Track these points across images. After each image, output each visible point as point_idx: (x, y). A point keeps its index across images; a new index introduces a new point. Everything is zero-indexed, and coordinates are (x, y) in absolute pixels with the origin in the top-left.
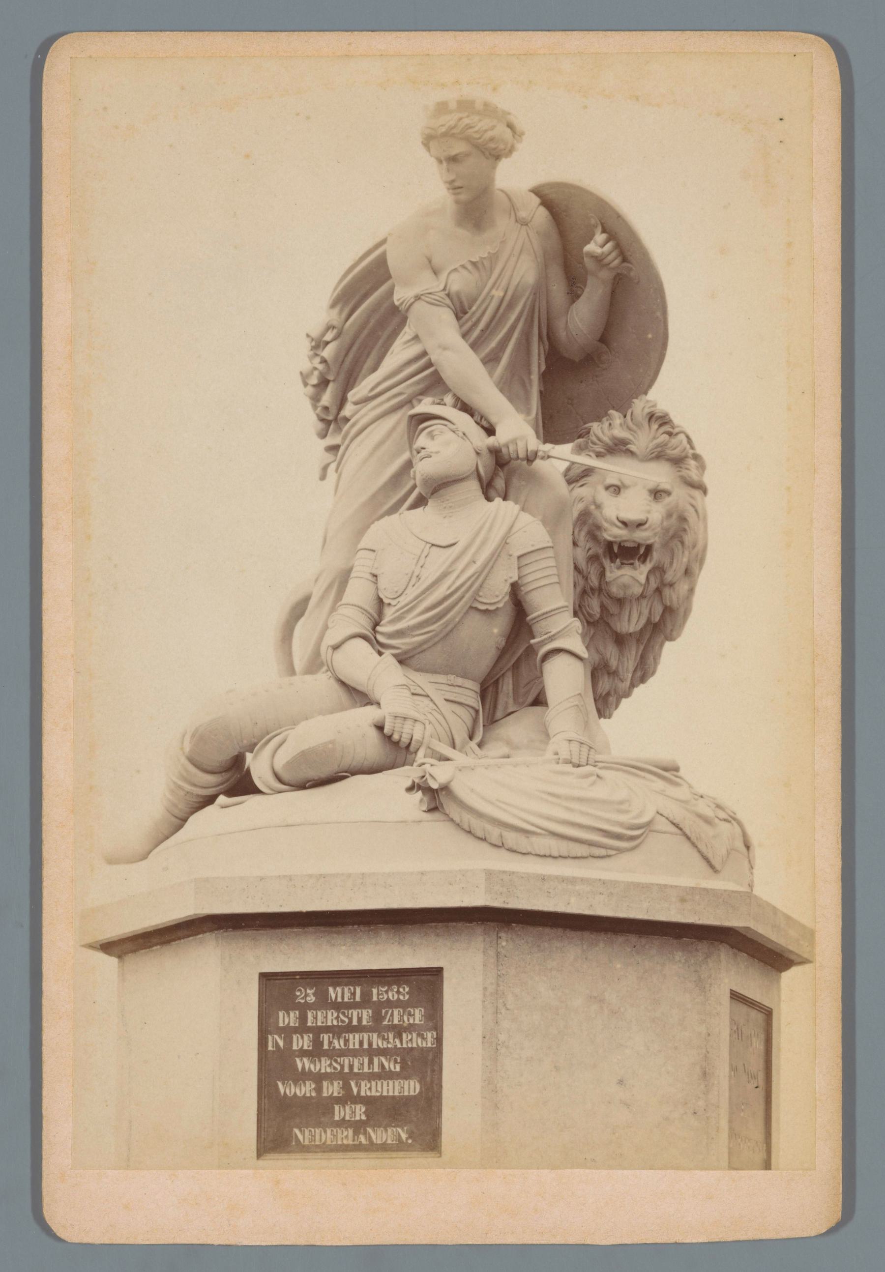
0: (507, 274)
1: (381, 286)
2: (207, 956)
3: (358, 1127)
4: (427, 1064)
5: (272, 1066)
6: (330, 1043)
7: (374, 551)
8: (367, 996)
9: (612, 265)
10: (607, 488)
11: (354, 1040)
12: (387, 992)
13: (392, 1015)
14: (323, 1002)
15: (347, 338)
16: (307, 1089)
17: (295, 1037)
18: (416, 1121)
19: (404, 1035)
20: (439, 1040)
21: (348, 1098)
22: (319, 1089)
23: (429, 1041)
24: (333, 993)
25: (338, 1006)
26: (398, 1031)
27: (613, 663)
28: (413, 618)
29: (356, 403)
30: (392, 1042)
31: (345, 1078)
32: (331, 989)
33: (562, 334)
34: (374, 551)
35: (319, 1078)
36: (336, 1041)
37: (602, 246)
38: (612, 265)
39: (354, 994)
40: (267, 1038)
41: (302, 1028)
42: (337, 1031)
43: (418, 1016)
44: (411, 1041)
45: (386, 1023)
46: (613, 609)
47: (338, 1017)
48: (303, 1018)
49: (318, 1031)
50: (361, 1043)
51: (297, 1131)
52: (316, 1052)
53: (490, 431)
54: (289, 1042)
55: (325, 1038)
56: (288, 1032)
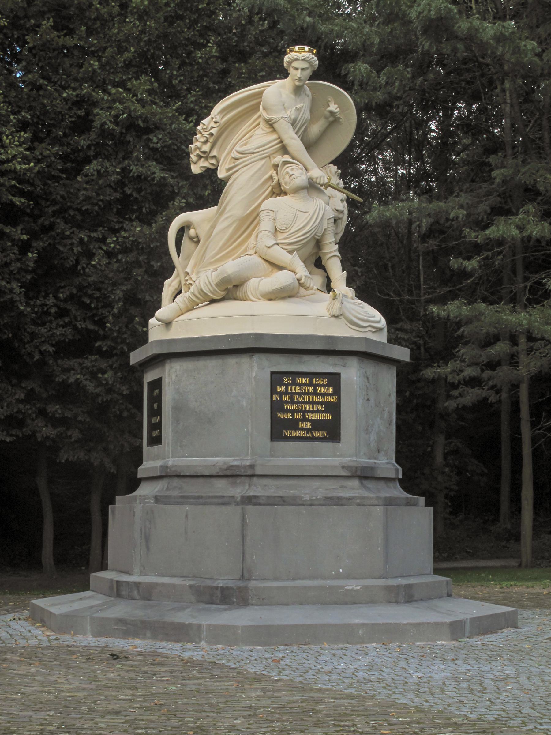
3: (308, 430)
4: (334, 409)
5: (276, 407)
16: (288, 416)
20: (339, 399)
21: (304, 420)
22: (293, 416)
23: (335, 399)
26: (324, 395)
31: (304, 412)
35: (293, 412)
49: (292, 394)
52: (292, 402)
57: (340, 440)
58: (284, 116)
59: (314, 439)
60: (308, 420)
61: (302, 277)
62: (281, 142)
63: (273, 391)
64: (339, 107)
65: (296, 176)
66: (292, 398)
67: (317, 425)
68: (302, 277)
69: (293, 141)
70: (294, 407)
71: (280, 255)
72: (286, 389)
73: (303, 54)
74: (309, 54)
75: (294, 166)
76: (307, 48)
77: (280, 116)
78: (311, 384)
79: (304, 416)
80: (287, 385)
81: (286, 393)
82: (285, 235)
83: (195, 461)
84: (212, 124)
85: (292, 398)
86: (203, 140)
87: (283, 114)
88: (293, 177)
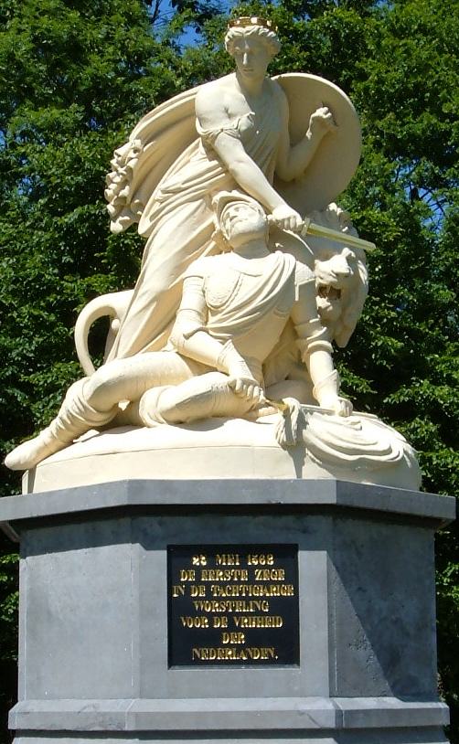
1: (191, 143)
3: (239, 648)
4: (288, 609)
5: (178, 608)
7: (202, 278)
15: (144, 158)
16: (203, 624)
18: (339, 713)
20: (296, 591)
21: (232, 628)
22: (211, 623)
23: (288, 592)
26: (267, 585)
28: (236, 319)
29: (165, 192)
31: (230, 617)
34: (202, 278)
35: (211, 616)
37: (326, 114)
43: (280, 576)
44: (274, 592)
45: (257, 579)
49: (208, 584)
51: (195, 650)
52: (209, 597)
53: (268, 212)
54: (188, 591)
57: (298, 664)
58: (227, 127)
59: (250, 662)
60: (239, 630)
61: (235, 381)
62: (227, 171)
63: (172, 579)
64: (329, 111)
65: (246, 217)
66: (209, 593)
67: (255, 638)
68: (235, 381)
69: (241, 164)
70: (216, 608)
71: (206, 346)
72: (198, 576)
73: (248, 28)
74: (257, 27)
75: (240, 204)
76: (254, 20)
77: (219, 128)
78: (243, 566)
79: (231, 623)
80: (199, 569)
81: (198, 582)
82: (219, 316)
83: (74, 705)
84: (132, 155)
85: (209, 593)
86: (118, 179)
87: (230, 124)
88: (235, 219)
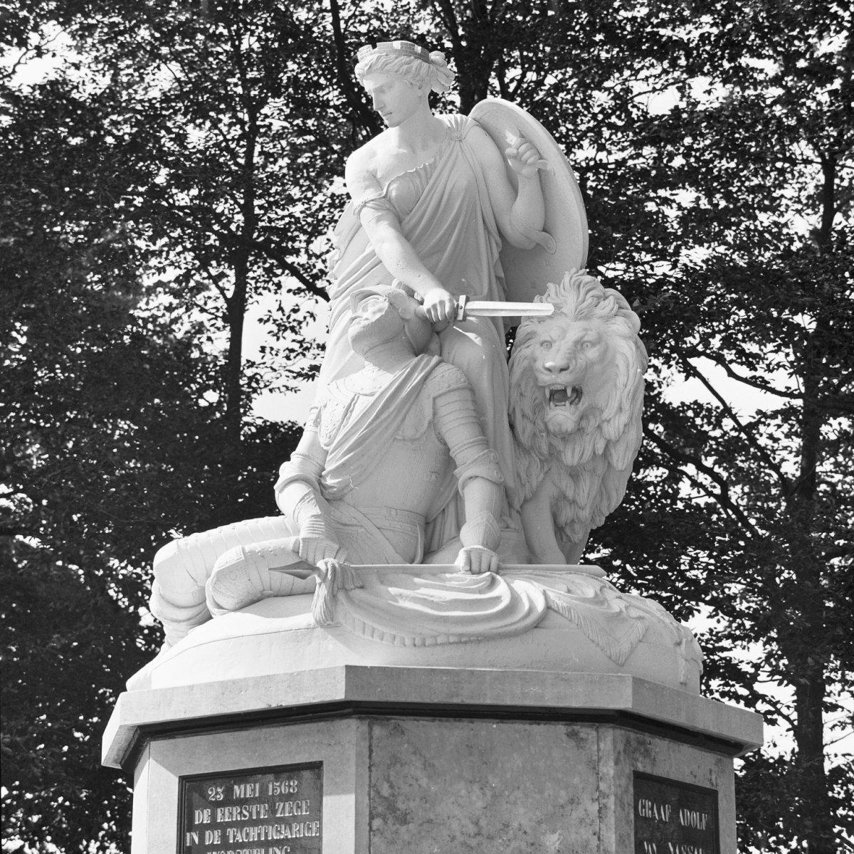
0: (445, 174)
2: (608, 741)
6: (235, 837)
8: (264, 790)
9: (529, 161)
10: (542, 344)
11: (254, 833)
12: (280, 786)
13: (284, 808)
14: (229, 801)
17: (207, 833)
19: (294, 825)
24: (239, 791)
25: (242, 802)
27: (570, 494)
30: (285, 834)
32: (236, 787)
33: (508, 230)
36: (239, 835)
38: (529, 161)
39: (253, 790)
40: (185, 836)
41: (213, 825)
42: (240, 825)
46: (558, 443)
47: (241, 812)
48: (213, 816)
49: (224, 826)
50: (259, 835)
55: (230, 832)
56: (202, 829)
66: (224, 837)
